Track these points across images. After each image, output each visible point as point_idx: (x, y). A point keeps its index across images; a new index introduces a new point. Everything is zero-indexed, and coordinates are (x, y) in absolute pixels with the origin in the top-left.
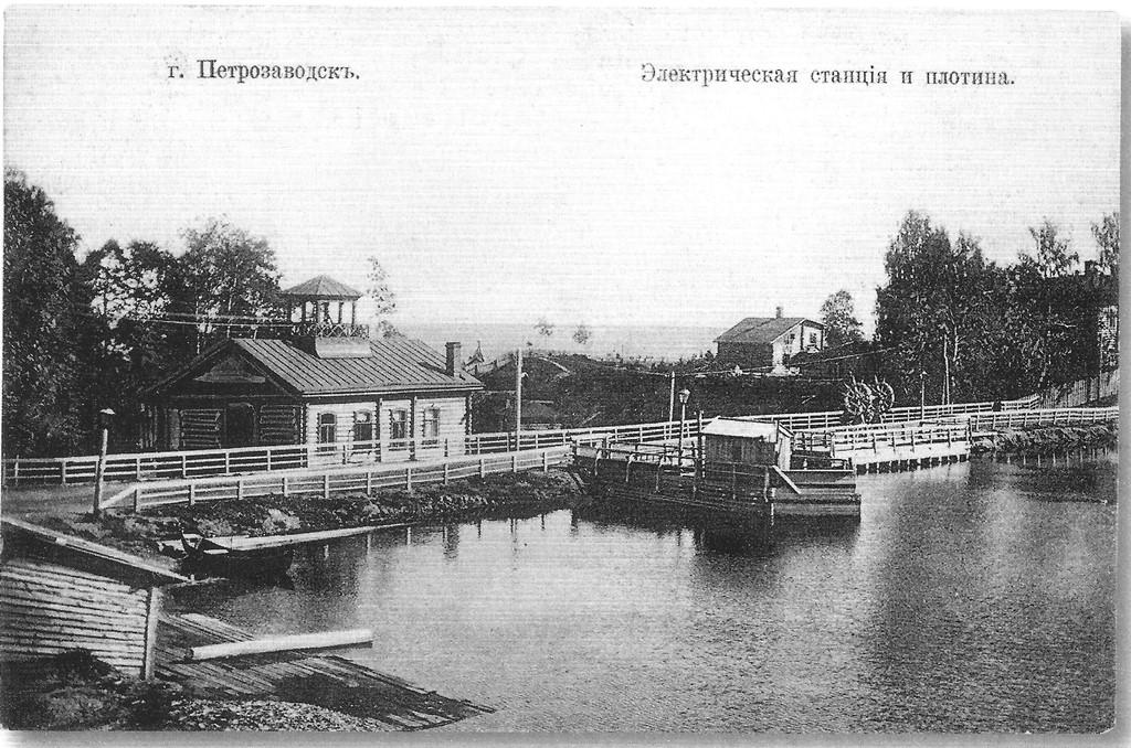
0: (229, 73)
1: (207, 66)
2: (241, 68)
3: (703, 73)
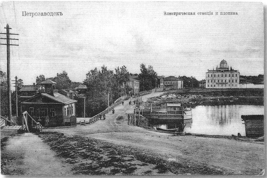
0: (29, 14)
1: (24, 13)
2: (33, 13)
3: (32, 14)
